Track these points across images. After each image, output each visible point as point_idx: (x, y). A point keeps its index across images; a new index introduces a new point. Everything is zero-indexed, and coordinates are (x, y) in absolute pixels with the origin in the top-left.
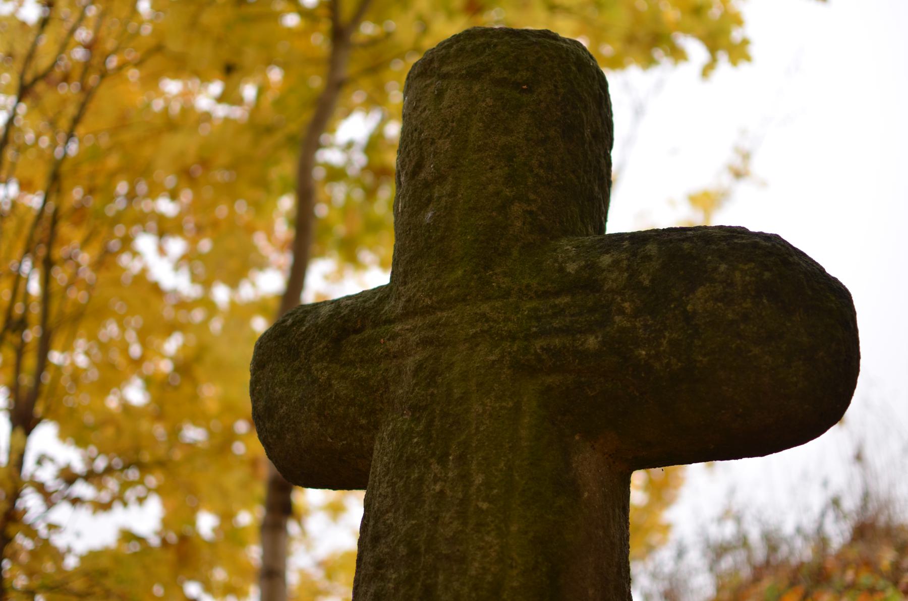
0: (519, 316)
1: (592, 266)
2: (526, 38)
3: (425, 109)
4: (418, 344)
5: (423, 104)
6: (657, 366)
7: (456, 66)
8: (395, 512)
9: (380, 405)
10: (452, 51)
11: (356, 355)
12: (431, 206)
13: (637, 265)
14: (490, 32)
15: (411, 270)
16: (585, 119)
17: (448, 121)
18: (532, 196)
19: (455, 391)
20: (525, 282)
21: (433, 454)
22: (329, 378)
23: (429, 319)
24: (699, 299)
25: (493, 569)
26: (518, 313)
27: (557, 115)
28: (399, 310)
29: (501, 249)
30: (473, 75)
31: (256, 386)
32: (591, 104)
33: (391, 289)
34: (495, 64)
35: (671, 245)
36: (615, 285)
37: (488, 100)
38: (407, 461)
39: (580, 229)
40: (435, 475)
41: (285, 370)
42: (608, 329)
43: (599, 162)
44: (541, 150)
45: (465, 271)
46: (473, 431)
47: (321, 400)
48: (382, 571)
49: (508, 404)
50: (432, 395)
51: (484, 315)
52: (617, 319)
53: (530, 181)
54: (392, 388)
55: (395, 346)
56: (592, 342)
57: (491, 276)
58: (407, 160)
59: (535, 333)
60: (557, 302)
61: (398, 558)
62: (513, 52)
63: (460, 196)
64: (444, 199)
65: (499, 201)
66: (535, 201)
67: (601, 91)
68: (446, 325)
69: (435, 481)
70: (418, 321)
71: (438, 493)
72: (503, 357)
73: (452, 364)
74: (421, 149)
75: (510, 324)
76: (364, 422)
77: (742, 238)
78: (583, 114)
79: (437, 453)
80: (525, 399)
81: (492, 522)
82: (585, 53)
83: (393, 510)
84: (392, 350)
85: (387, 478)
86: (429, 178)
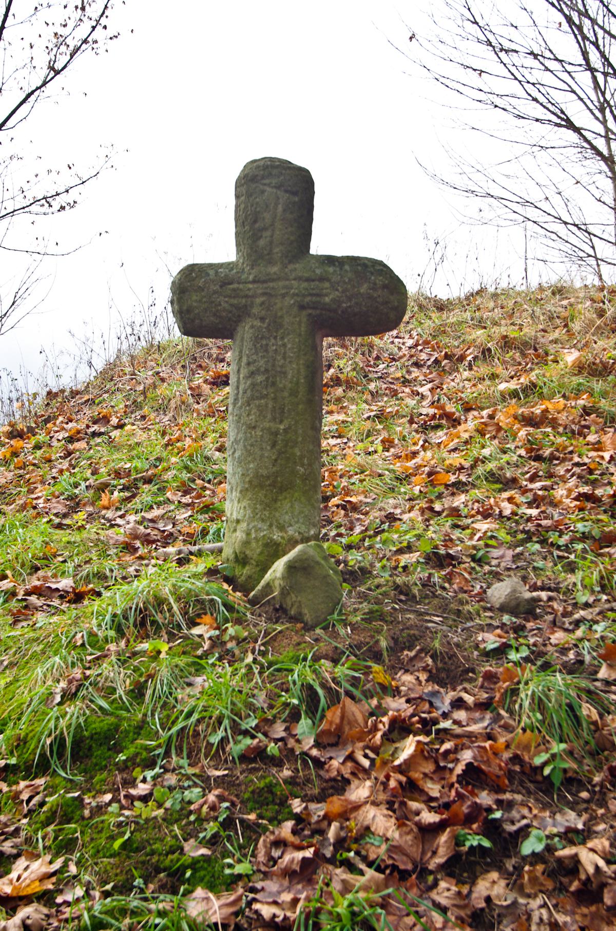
23: (265, 285)
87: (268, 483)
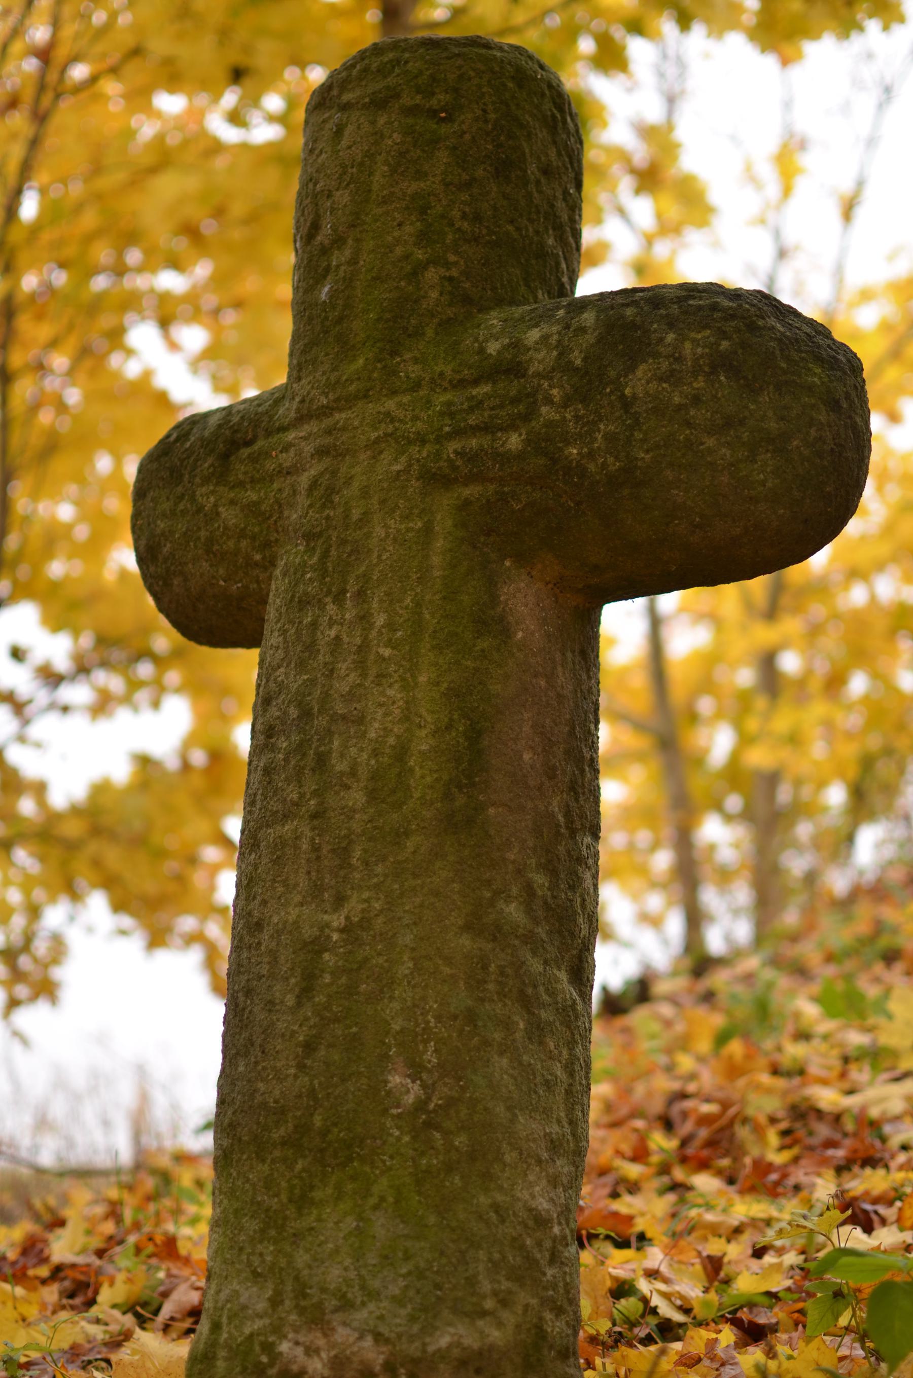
0: (430, 412)
1: (516, 345)
2: (446, 49)
3: (321, 152)
4: (312, 455)
5: (320, 146)
6: (592, 467)
7: (358, 93)
8: (287, 666)
9: (275, 534)
10: (355, 72)
11: (245, 473)
12: (329, 277)
13: (569, 340)
14: (402, 44)
15: (306, 362)
16: (527, 151)
17: (347, 166)
18: (452, 258)
19: (354, 511)
20: (438, 369)
21: (329, 592)
22: (216, 505)
23: (327, 422)
24: (640, 379)
25: (396, 730)
26: (429, 408)
27: (486, 148)
28: (293, 414)
29: (411, 328)
30: (379, 103)
31: (137, 520)
32: (538, 130)
33: (286, 388)
34: (404, 87)
35: (611, 312)
36: (541, 368)
37: (395, 135)
38: (300, 602)
39: (523, 296)
40: (331, 618)
41: (168, 499)
42: (533, 423)
43: (552, 206)
44: (465, 197)
45: (367, 359)
46: (375, 561)
47: (208, 533)
48: (273, 740)
49: (416, 524)
50: (328, 518)
51: (388, 414)
52: (544, 410)
53: (450, 238)
54: (286, 513)
55: (287, 459)
56: (514, 441)
57: (399, 363)
58: (302, 219)
59: (448, 433)
60: (474, 393)
61: (289, 722)
62: (427, 69)
63: (362, 263)
64: (343, 268)
65: (409, 267)
66: (456, 263)
67: (556, 112)
68: (344, 429)
69: (331, 624)
70: (312, 427)
71: (333, 639)
72: (410, 465)
73: (351, 478)
74: (317, 205)
75: (419, 424)
76: (258, 557)
77: (701, 298)
78: (525, 144)
79: (333, 590)
80: (439, 517)
81: (395, 672)
82: (530, 63)
83: (285, 665)
84: (285, 465)
85: (279, 625)
86: (326, 242)
87: (278, 1134)
